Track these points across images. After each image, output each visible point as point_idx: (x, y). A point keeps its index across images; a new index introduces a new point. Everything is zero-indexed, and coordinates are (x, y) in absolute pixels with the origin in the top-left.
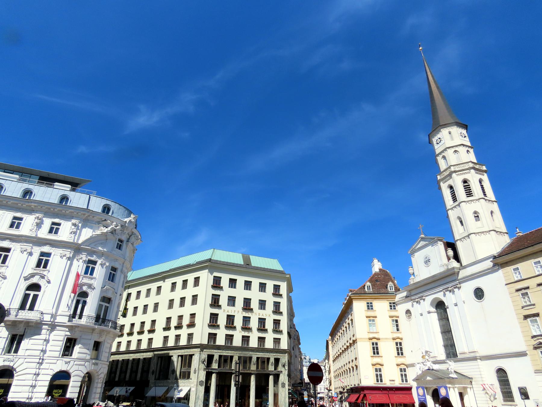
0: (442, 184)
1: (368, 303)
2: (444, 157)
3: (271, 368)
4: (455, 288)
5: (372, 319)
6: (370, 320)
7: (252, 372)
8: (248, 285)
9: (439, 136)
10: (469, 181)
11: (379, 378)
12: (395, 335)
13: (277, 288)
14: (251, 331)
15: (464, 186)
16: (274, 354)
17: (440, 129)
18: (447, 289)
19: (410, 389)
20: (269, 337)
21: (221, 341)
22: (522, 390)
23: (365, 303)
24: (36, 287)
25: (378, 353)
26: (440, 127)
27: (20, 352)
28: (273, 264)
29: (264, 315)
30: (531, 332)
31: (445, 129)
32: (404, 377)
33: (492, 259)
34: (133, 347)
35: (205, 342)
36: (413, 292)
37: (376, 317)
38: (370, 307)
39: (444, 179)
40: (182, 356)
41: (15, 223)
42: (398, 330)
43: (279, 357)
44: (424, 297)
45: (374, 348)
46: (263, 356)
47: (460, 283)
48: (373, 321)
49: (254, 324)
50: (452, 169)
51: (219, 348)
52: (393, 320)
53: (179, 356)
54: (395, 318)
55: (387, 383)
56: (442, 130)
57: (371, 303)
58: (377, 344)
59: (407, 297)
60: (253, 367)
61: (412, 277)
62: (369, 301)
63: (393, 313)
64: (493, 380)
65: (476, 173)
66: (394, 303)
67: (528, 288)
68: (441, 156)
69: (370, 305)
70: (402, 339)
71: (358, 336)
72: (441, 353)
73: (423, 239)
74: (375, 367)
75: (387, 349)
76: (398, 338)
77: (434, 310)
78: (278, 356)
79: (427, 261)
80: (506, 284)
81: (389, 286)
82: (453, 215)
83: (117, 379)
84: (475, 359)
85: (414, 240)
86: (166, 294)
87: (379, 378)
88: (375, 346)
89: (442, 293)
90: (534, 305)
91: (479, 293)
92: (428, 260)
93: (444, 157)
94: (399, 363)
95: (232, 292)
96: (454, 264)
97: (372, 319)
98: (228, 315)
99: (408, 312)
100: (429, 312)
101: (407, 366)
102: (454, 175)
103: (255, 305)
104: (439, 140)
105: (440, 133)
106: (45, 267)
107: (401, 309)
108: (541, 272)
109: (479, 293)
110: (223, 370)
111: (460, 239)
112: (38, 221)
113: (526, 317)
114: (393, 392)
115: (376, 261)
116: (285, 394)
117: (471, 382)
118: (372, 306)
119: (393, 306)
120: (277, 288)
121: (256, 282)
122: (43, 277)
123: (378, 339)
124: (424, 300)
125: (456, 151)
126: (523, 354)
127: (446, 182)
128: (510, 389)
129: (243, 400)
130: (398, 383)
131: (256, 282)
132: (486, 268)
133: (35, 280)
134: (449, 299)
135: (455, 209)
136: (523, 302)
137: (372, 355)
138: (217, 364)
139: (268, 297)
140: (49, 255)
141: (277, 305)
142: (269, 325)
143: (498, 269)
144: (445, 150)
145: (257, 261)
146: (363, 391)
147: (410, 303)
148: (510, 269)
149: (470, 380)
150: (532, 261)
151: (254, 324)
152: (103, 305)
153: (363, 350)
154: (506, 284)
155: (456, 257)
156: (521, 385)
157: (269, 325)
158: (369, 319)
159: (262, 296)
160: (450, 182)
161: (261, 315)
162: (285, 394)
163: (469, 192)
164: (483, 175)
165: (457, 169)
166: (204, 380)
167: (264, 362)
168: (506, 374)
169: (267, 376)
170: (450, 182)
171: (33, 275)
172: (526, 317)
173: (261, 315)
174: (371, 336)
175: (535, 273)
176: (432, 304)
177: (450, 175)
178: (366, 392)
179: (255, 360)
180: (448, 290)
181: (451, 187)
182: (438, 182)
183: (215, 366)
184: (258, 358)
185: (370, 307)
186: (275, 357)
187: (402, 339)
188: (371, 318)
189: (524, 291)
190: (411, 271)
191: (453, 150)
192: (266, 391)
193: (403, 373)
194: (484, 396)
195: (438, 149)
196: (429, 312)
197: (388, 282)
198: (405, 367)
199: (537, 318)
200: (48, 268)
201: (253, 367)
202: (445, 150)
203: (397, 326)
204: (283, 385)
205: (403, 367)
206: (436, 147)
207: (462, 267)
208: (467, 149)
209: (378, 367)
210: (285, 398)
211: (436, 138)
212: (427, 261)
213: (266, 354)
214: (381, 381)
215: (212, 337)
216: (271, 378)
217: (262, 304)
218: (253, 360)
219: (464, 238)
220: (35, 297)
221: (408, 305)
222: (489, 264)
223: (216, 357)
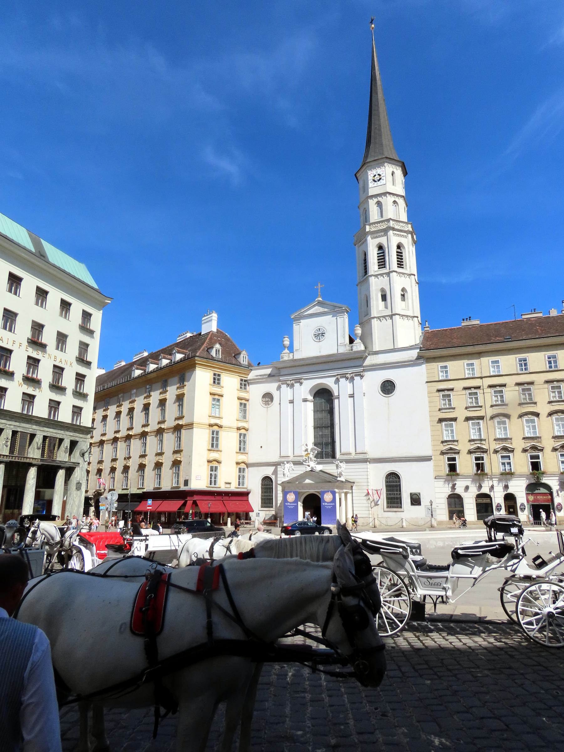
0: (369, 238)
1: (215, 374)
2: (379, 204)
4: (356, 375)
5: (216, 398)
6: (214, 399)
9: (379, 171)
10: (404, 248)
11: (213, 478)
12: (241, 424)
13: (86, 316)
14: (40, 388)
16: (71, 434)
17: (384, 162)
18: (344, 376)
19: (247, 494)
20: (67, 402)
22: (414, 497)
23: (212, 373)
26: (385, 160)
28: (79, 270)
29: (63, 362)
30: (443, 437)
31: (390, 165)
32: (241, 479)
36: (283, 372)
37: (222, 396)
38: (216, 380)
39: (375, 234)
42: (245, 417)
43: (77, 439)
44: (302, 381)
45: (213, 438)
46: (55, 435)
47: (364, 371)
48: (218, 400)
49: (45, 373)
50: (392, 223)
52: (241, 404)
54: (243, 402)
55: (222, 486)
56: (386, 164)
57: (219, 375)
58: (217, 433)
59: (270, 375)
61: (286, 351)
62: (218, 371)
63: (243, 395)
64: (381, 485)
66: (245, 381)
67: (504, 385)
68: (375, 200)
69: (217, 377)
71: (196, 420)
73: (320, 304)
74: (211, 465)
75: (229, 440)
76: (244, 428)
77: (311, 398)
78: (76, 436)
79: (320, 335)
80: (427, 382)
82: (375, 285)
84: (365, 461)
85: (308, 301)
87: (213, 478)
88: (215, 436)
89: (334, 378)
90: (454, 408)
92: (317, 334)
93: (379, 204)
94: (240, 461)
97: (216, 398)
99: (268, 397)
100: (305, 400)
101: (248, 465)
102: (391, 233)
103: (48, 337)
104: (377, 177)
105: (383, 168)
107: (256, 392)
109: (388, 387)
111: (378, 318)
113: (441, 420)
114: (227, 498)
115: (214, 316)
116: (80, 501)
117: (352, 487)
118: (219, 380)
119: (244, 384)
120: (86, 316)
121: (55, 296)
123: (220, 427)
124: (301, 384)
125: (395, 202)
126: (427, 459)
127: (377, 237)
128: (400, 494)
130: (233, 487)
131: (55, 296)
132: (406, 359)
134: (341, 389)
135: (381, 278)
136: (439, 402)
142: (68, 381)
143: (422, 363)
144: (385, 194)
145: (56, 256)
146: (192, 496)
147: (276, 385)
148: (436, 366)
150: (466, 362)
151: (45, 373)
153: (199, 439)
154: (427, 382)
156: (414, 491)
157: (68, 381)
158: (213, 397)
160: (383, 240)
161: (58, 360)
162: (80, 501)
165: (396, 227)
168: (399, 478)
170: (383, 240)
172: (441, 420)
173: (58, 360)
174: (213, 421)
175: (490, 373)
176: (310, 391)
177: (385, 231)
178: (196, 498)
179: (41, 441)
181: (380, 247)
182: (366, 234)
184: (45, 438)
185: (216, 380)
186: (72, 438)
187: (247, 430)
188: (216, 397)
189: (446, 393)
190: (287, 342)
194: (365, 502)
195: (373, 189)
196: (305, 400)
198: (245, 467)
199: (453, 423)
202: (385, 194)
203: (245, 411)
205: (243, 466)
206: (371, 184)
209: (215, 464)
210: (79, 507)
211: (374, 172)
212: (320, 335)
213: (60, 432)
217: (62, 338)
219: (384, 317)
221: (271, 387)
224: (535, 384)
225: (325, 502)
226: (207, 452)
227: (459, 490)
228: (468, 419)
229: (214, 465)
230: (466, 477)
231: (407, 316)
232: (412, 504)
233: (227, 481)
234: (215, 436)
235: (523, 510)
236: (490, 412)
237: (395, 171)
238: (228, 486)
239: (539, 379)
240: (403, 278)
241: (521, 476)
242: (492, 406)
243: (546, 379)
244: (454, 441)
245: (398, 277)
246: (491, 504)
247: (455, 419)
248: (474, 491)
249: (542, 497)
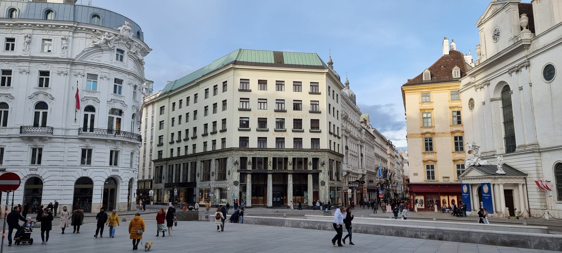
3: (310, 168)
7: (289, 172)
8: (280, 85)
11: (430, 174)
12: (455, 129)
13: (314, 87)
21: (253, 143)
24: (42, 105)
25: (431, 149)
27: (43, 163)
34: (175, 154)
35: (237, 145)
40: (218, 159)
41: (10, 43)
51: (252, 150)
53: (216, 159)
55: (439, 179)
60: (290, 168)
70: (463, 132)
72: (500, 146)
83: (174, 182)
86: (202, 102)
87: (430, 174)
88: (428, 142)
91: (549, 72)
95: (262, 94)
96: (526, 35)
98: (294, 119)
106: (47, 86)
110: (277, 171)
112: (27, 39)
116: (325, 192)
120: (314, 87)
122: (46, 95)
129: (285, 198)
133: (41, 98)
137: (424, 151)
138: (251, 166)
139: (306, 98)
140: (9, 72)
141: (314, 104)
152: (113, 118)
159: (298, 96)
166: (238, 180)
167: (298, 162)
169: (305, 175)
171: (37, 94)
174: (425, 131)
179: (292, 160)
180: (514, 71)
183: (249, 168)
187: (463, 132)
192: (305, 188)
193: (430, 170)
200: (49, 86)
201: (290, 168)
204: (323, 183)
207: (536, 38)
214: (433, 178)
215: (244, 141)
216: (310, 177)
218: (289, 160)
220: (45, 115)
223: (250, 159)
225: (484, 193)
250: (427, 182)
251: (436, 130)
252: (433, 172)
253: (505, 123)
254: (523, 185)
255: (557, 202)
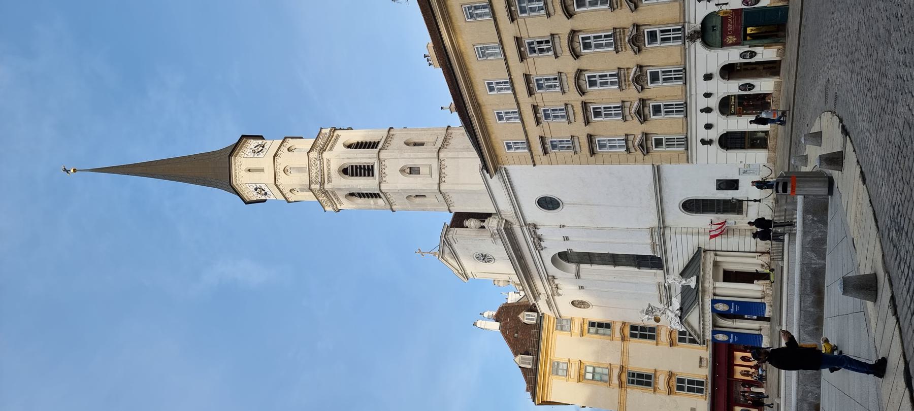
12: (617, 334)
15: (352, 175)
33: (488, 175)
55: (703, 373)
64: (703, 220)
65: (331, 149)
70: (624, 323)
72: (650, 276)
81: (526, 321)
88: (635, 379)
91: (548, 203)
96: (492, 223)
102: (327, 186)
108: (541, 4)
109: (548, 203)
117: (705, 251)
119: (561, 323)
137: (651, 389)
149: (699, 254)
154: (534, 165)
155: (482, 217)
163: (366, 171)
164: (338, 136)
172: (592, 152)
174: (615, 381)
191: (280, 174)
196: (578, 276)
197: (519, 321)
208: (284, 149)
214: (701, 383)
222: (495, 182)
224: (519, 36)
225: (728, 340)
226: (657, 394)
227: (714, 134)
228: (587, 122)
229: (678, 336)
230: (687, 126)
231: (440, 169)
232: (737, 189)
233: (698, 364)
234: (635, 379)
235: (753, 54)
236: (573, 97)
237: (244, 167)
238: (704, 363)
239: (509, 30)
240: (387, 171)
241: (685, 56)
242: (564, 92)
243: (508, 21)
244: (626, 140)
245: (387, 179)
246: (740, 96)
247: (590, 137)
248: (714, 117)
249: (730, 25)
250: (709, 395)
251: (617, 363)
252: (691, 382)
253: (615, 265)
254: (716, 255)
255: (744, 215)
